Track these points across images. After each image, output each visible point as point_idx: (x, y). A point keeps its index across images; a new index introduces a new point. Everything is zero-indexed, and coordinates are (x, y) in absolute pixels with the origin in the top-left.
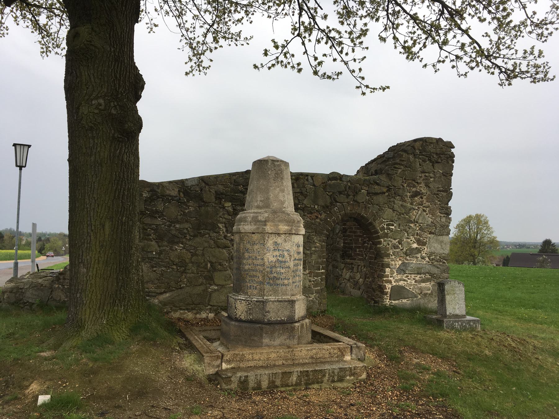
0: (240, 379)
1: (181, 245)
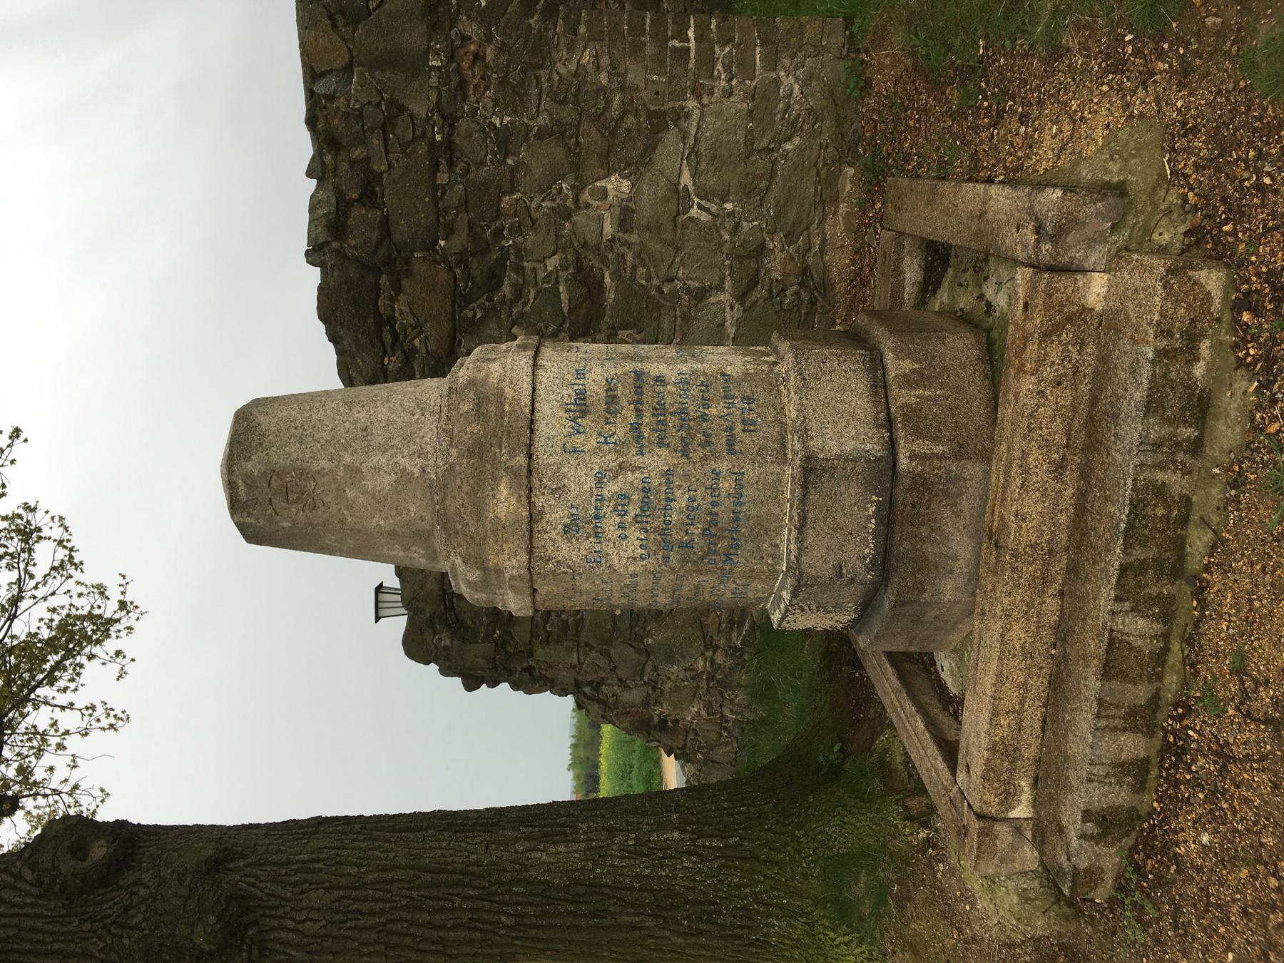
0: (1092, 838)
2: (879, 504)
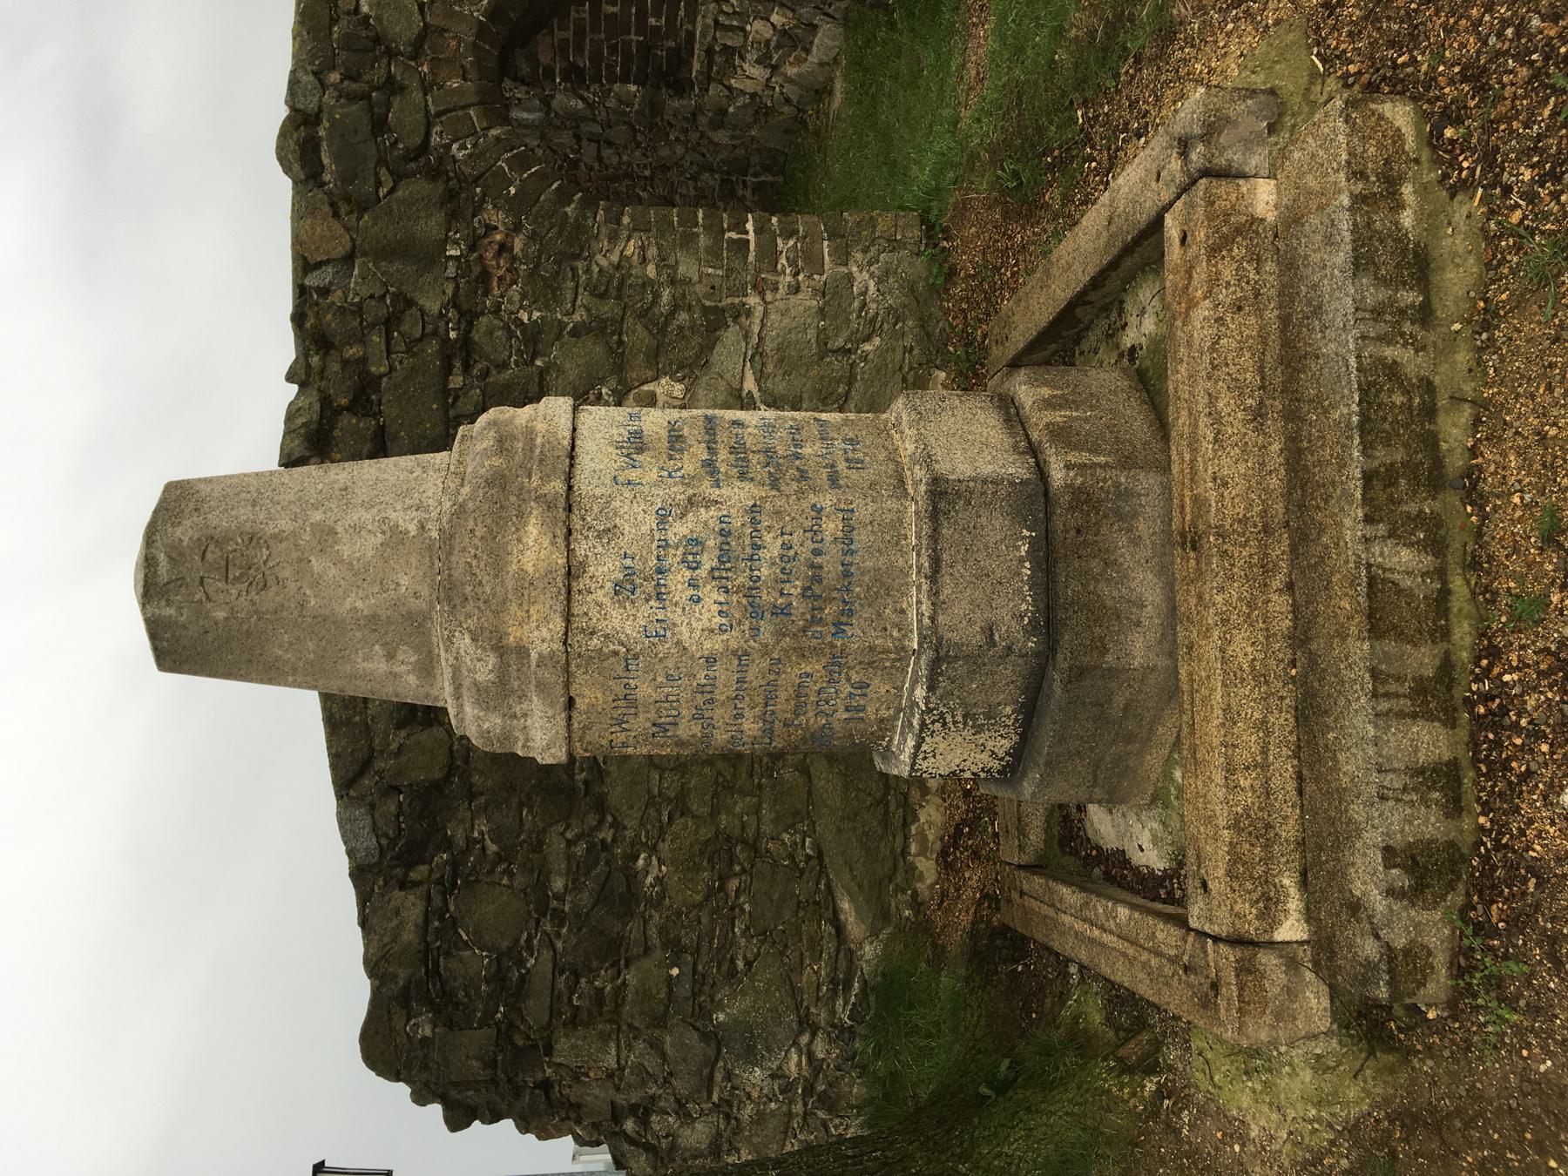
1: (641, 862)
2: (1033, 542)
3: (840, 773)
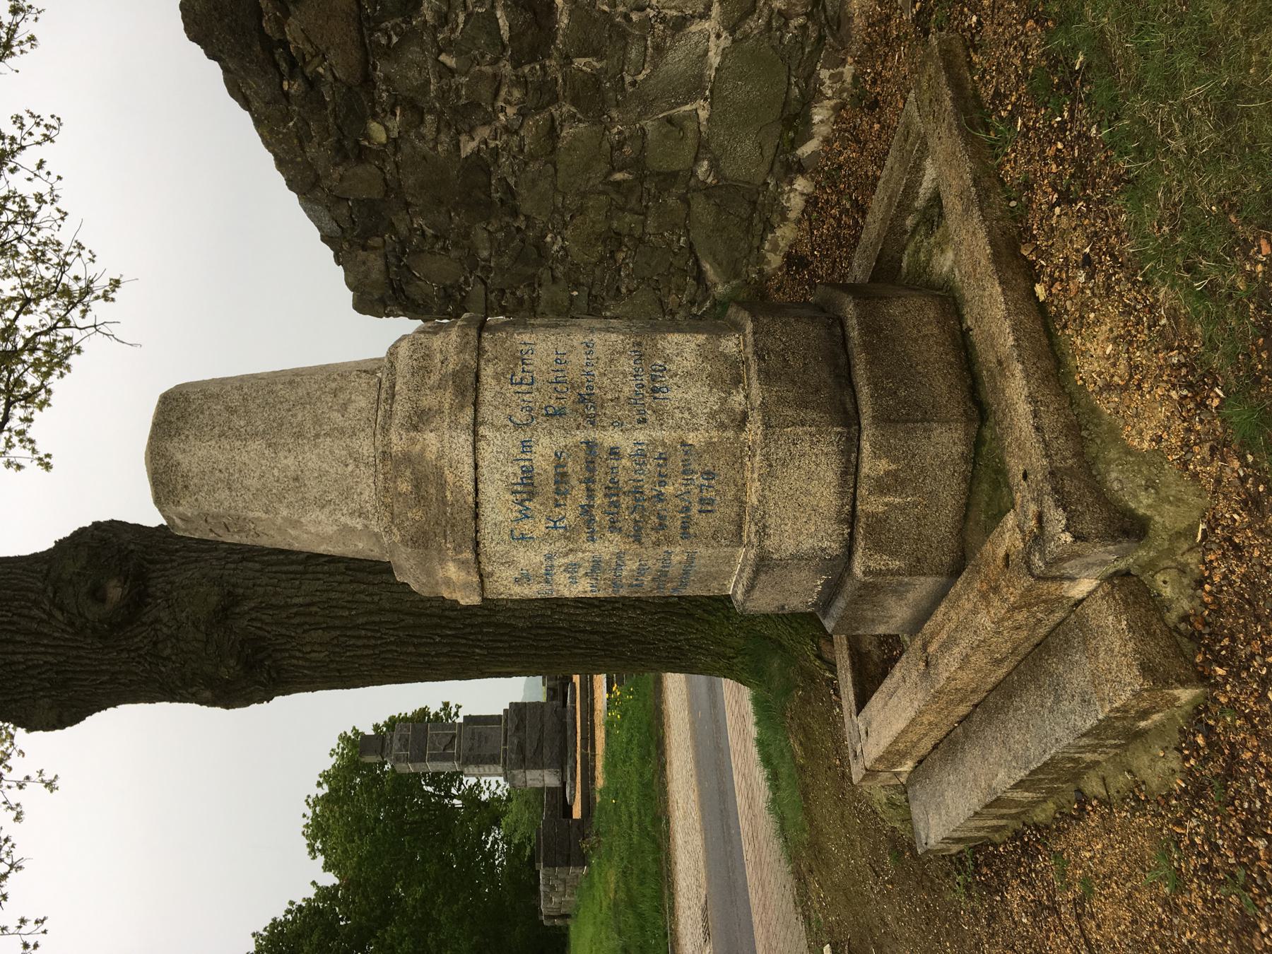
3: (716, 204)
